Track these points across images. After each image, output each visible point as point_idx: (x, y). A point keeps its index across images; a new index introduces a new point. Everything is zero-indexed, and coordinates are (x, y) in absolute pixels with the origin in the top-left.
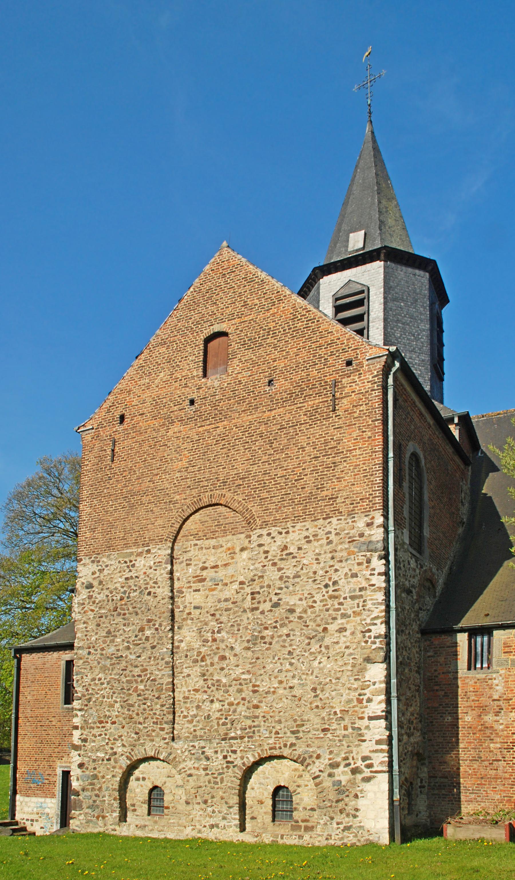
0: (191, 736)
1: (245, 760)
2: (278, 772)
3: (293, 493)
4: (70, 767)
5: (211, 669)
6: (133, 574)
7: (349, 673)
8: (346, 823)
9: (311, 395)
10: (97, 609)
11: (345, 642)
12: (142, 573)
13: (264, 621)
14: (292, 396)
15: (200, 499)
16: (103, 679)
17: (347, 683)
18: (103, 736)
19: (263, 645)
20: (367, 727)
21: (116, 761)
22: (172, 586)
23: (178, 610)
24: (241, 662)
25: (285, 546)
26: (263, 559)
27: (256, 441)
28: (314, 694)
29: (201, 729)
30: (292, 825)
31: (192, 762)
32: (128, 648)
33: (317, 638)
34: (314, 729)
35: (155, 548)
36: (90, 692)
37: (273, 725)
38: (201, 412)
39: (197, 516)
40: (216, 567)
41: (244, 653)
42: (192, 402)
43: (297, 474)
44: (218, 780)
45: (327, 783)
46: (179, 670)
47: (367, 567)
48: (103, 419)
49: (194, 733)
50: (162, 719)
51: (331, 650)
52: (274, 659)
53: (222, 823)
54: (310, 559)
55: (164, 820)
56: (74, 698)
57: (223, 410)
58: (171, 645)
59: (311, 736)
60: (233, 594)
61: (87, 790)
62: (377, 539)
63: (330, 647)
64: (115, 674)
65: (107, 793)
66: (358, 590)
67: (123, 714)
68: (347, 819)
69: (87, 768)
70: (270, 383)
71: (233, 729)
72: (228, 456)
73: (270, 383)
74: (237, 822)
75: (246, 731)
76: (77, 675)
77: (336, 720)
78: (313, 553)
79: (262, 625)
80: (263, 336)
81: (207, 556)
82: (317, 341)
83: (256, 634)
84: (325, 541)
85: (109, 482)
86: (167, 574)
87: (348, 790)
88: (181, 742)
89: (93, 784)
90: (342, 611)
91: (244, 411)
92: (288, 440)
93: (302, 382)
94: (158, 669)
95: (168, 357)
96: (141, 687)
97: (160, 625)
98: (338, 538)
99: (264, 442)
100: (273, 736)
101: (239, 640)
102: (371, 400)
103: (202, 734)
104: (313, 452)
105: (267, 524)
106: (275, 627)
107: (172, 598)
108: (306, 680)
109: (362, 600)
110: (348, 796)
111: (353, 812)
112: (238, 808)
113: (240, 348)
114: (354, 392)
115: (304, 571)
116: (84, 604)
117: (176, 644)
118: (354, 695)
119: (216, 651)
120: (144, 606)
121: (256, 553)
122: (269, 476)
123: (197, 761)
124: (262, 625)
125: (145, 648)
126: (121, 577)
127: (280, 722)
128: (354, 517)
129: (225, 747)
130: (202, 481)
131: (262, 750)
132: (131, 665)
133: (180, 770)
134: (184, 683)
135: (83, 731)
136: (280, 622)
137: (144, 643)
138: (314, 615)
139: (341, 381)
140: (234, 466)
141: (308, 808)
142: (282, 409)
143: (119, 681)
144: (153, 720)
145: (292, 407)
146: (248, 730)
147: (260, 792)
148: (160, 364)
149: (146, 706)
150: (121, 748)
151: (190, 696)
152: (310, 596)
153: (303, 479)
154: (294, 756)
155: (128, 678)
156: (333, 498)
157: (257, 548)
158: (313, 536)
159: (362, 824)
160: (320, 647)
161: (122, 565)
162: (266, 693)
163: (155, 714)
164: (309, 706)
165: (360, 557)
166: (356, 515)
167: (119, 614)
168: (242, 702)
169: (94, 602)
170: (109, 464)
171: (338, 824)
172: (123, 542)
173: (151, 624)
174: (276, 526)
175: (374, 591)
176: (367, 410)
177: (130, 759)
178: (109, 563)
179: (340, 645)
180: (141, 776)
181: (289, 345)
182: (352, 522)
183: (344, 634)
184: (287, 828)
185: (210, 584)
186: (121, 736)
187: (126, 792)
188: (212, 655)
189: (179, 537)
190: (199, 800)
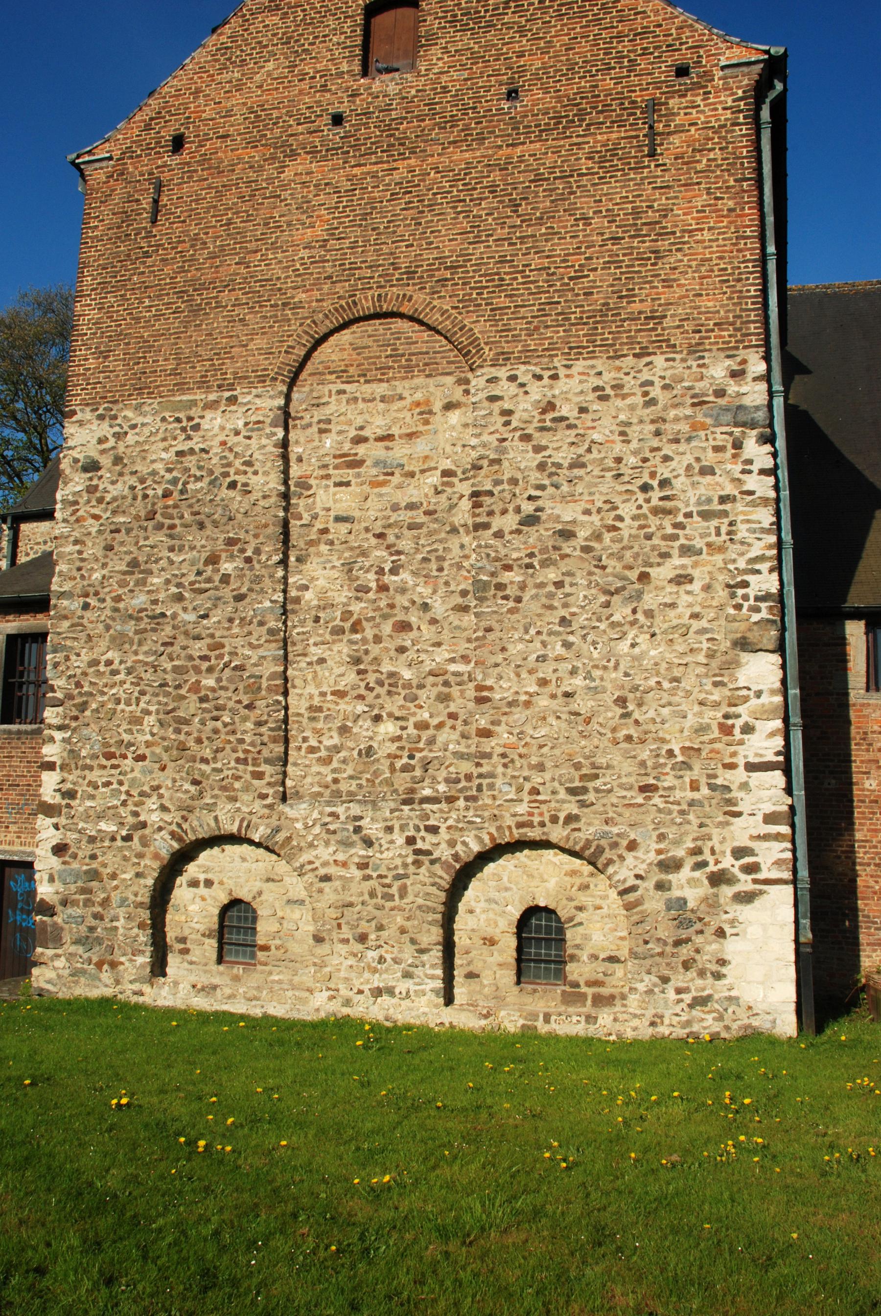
0: (327, 793)
1: (459, 848)
2: (531, 876)
3: (566, 301)
4: (32, 854)
5: (375, 650)
6: (196, 444)
7: (701, 670)
8: (696, 990)
9: (602, 123)
10: (108, 514)
11: (690, 605)
12: (216, 442)
13: (503, 552)
14: (560, 123)
15: (355, 303)
16: (117, 662)
17: (697, 689)
18: (115, 786)
19: (500, 602)
20: (744, 786)
21: (144, 842)
22: (286, 472)
23: (299, 523)
24: (446, 635)
25: (549, 402)
26: (499, 426)
27: (481, 199)
28: (620, 711)
29: (351, 777)
30: (564, 992)
31: (332, 849)
32: (179, 598)
33: (626, 593)
34: (621, 786)
35: (249, 393)
36: (86, 689)
37: (526, 773)
38: (359, 140)
39: (346, 336)
40: (389, 437)
41: (455, 619)
42: (338, 120)
43: (573, 266)
44: (394, 890)
45: (654, 903)
46: (299, 648)
47: (734, 456)
48: (134, 142)
49: (334, 787)
50: (259, 752)
51: (658, 620)
52: (527, 631)
53: (402, 986)
54: (607, 432)
55: (256, 975)
56: (47, 702)
57: (407, 138)
58: (281, 594)
59: (615, 800)
60: (426, 495)
61: (75, 903)
62: (755, 404)
63: (656, 613)
64: (146, 653)
65: (122, 912)
66: (716, 500)
67: (164, 739)
68: (699, 982)
69: (75, 856)
70: (512, 94)
71: (427, 781)
72: (420, 224)
73: (512, 94)
74: (439, 984)
75: (460, 786)
76: (55, 651)
77: (673, 769)
78: (612, 420)
79: (497, 559)
80: (493, 10)
81: (367, 416)
82: (613, 27)
83: (485, 578)
84: (639, 400)
85: (145, 263)
86: (275, 446)
87: (701, 919)
88: (304, 806)
89: (89, 892)
90: (682, 541)
91: (455, 142)
92: (552, 202)
93: (582, 98)
94: (250, 644)
95: (284, 34)
96: (210, 682)
97: (257, 551)
98: (668, 394)
99: (499, 202)
100: (526, 798)
102: (733, 142)
103: (353, 788)
104: (609, 228)
105: (509, 359)
106: (529, 566)
107: (286, 496)
108: (602, 679)
109: (726, 521)
110: (701, 932)
111: (714, 967)
112: (440, 954)
113: (445, 28)
114: (696, 124)
115: (595, 455)
116: (76, 503)
117: (293, 593)
118: (713, 717)
119: (386, 611)
120: (220, 511)
121: (483, 412)
122: (510, 267)
123: (341, 848)
124: (497, 559)
125: (219, 599)
126: (165, 450)
127: (541, 767)
128: (703, 358)
129: (410, 818)
130: (360, 268)
131: (499, 828)
132: (186, 633)
133: (302, 866)
135: (66, 775)
136: (539, 557)
137: (216, 589)
138: (618, 546)
139: (667, 104)
140: (432, 243)
141: (602, 956)
142: (538, 145)
143: (154, 667)
144: (235, 755)
145: (562, 143)
146: (463, 784)
147: (488, 920)
148: (266, 46)
149: (219, 724)
150: (157, 813)
151: (326, 706)
152: (608, 506)
153: (587, 276)
154: (576, 843)
155: (176, 663)
156: (656, 318)
157: (486, 404)
158: (613, 387)
159: (733, 993)
160: (634, 611)
161: (170, 427)
162: (510, 704)
164: (609, 735)
165: (718, 436)
166: (706, 354)
167: (159, 527)
168: (450, 722)
169: (100, 500)
170: (145, 228)
171: (679, 991)
172: (172, 381)
173: (236, 548)
174: (529, 363)
175: (753, 504)
176: (723, 159)
177: (180, 840)
178: (140, 420)
179: (680, 610)
180: (202, 877)
181: (553, 30)
182: (699, 366)
183: (688, 587)
184: (553, 999)
185: (374, 472)
186: (158, 787)
187: (165, 911)
188: (378, 620)
189: (304, 375)
190: (346, 932)
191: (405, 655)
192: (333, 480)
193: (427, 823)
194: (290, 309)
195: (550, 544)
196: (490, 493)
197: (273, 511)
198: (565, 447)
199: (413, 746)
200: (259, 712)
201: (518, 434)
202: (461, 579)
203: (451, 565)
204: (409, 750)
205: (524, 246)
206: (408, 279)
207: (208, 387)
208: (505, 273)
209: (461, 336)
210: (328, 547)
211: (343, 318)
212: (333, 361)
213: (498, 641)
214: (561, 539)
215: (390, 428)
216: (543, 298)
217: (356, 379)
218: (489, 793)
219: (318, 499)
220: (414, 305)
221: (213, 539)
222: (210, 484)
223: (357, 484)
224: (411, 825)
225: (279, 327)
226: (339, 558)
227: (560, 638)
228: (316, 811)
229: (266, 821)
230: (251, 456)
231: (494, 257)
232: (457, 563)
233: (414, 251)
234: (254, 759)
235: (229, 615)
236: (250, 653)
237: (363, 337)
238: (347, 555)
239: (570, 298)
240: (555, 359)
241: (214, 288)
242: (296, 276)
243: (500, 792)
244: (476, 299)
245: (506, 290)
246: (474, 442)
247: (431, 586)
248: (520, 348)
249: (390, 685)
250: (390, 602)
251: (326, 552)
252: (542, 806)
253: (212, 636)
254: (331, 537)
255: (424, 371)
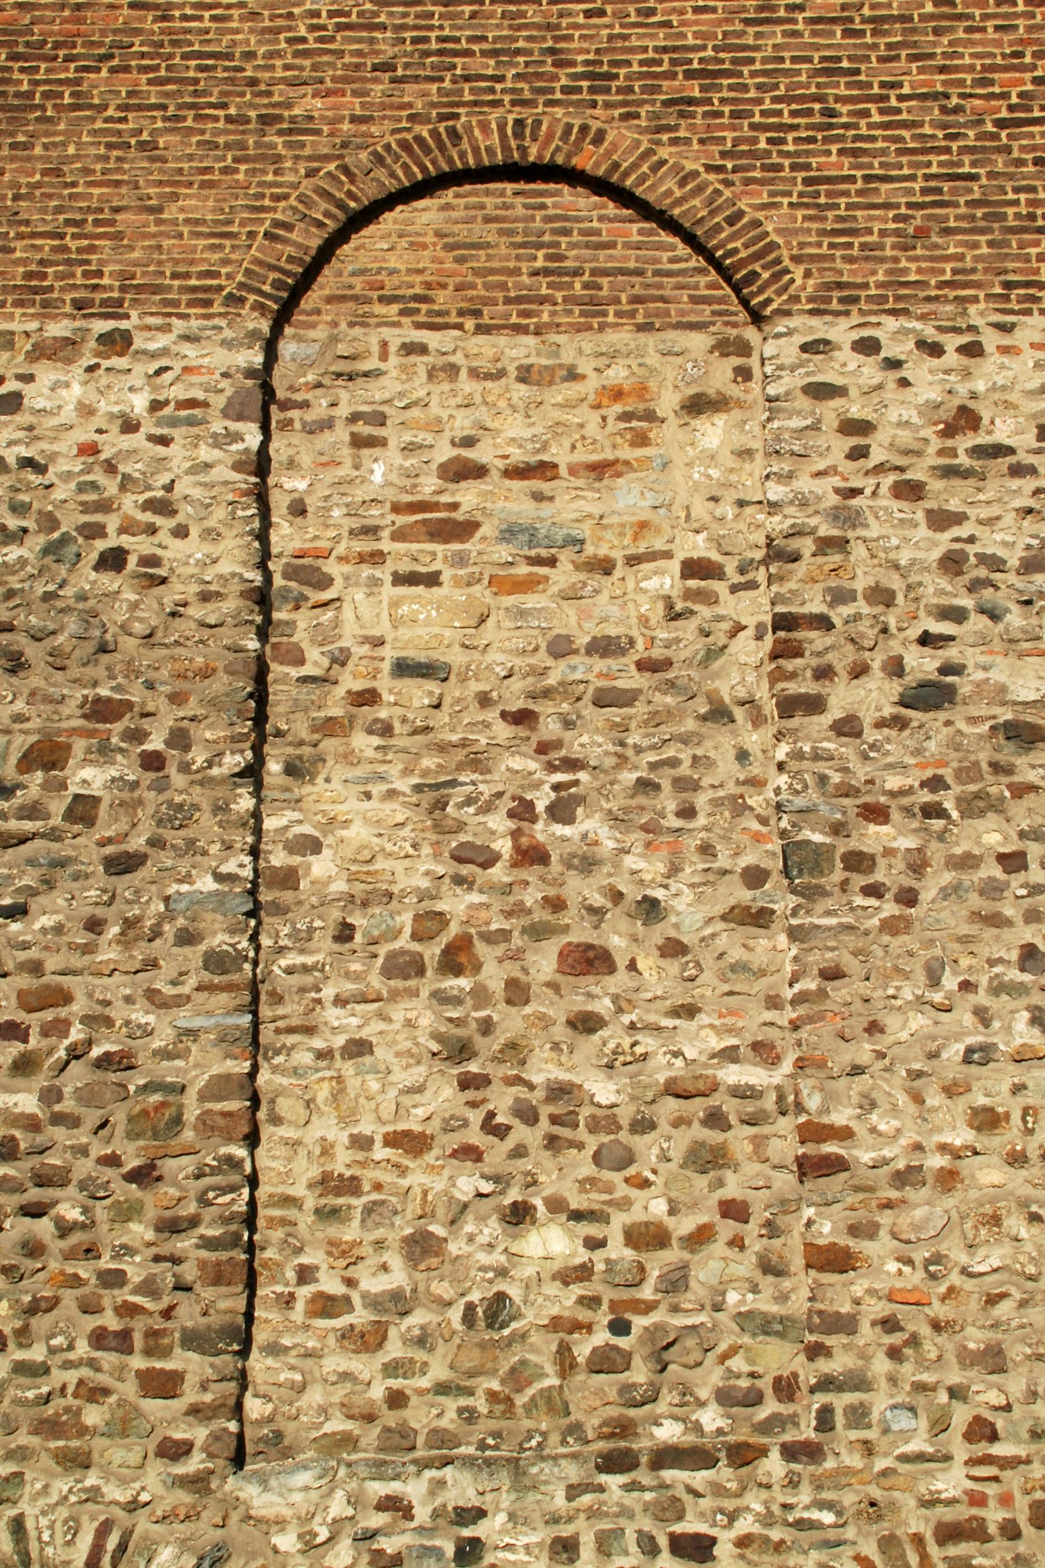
0: (371, 1436)
3: (991, 175)
12: (67, 445)
13: (861, 772)
15: (453, 133)
19: (859, 900)
22: (263, 536)
23: (294, 672)
29: (443, 1389)
35: (166, 329)
37: (955, 1377)
43: (1005, 96)
46: (292, 1010)
49: (391, 1418)
50: (167, 1313)
52: (934, 981)
58: (247, 859)
60: (644, 621)
71: (668, 1398)
75: (763, 1413)
79: (847, 791)
81: (482, 414)
83: (817, 838)
86: (238, 467)
88: (304, 1478)
94: (152, 995)
97: (180, 739)
100: (961, 1451)
101: (693, 868)
103: (449, 1421)
105: (856, 300)
117: (278, 858)
120: (72, 625)
121: (796, 423)
122: (849, 85)
124: (847, 791)
125: (61, 863)
129: (627, 1513)
130: (467, 53)
134: (323, 1093)
136: (957, 789)
137: (53, 835)
140: (652, 12)
144: (91, 1322)
146: (771, 1407)
149: (44, 1227)
151: (369, 1176)
157: (803, 402)
162: (905, 1178)
163: (114, 1279)
168: (727, 1228)
173: (118, 727)
174: (906, 312)
189: (311, 299)
191: (596, 1038)
192: (390, 567)
193: (678, 1528)
194: (280, 133)
195: (983, 757)
196: (824, 623)
197: (228, 636)
198: (1009, 519)
199: (625, 1294)
200: (173, 1192)
201: (888, 480)
202: (745, 839)
203: (716, 802)
204: (614, 1305)
205: (883, 41)
206: (592, 90)
207: (45, 304)
208: (838, 99)
209: (733, 237)
210: (376, 741)
211: (423, 169)
212: (392, 272)
213: (858, 1006)
214: (1010, 747)
215: (545, 447)
216: (936, 164)
217: (454, 319)
218: (854, 1435)
219: (347, 613)
220: (608, 153)
221: (49, 700)
222: (46, 551)
223: (457, 582)
224: (631, 1536)
225: (253, 172)
226: (407, 772)
227: (1024, 1001)
228: (339, 1494)
229: (181, 1529)
230: (169, 488)
231: (809, 60)
232: (733, 798)
233: (605, 28)
234: (152, 1334)
235: (89, 911)
236: (151, 1018)
237: (472, 220)
238: (428, 762)
239: (1000, 167)
240: (972, 309)
241: (68, 59)
242: (297, 54)
243: (886, 1431)
244: (768, 153)
245: (840, 138)
246: (776, 492)
247: (664, 853)
248: (881, 277)
249: (554, 1120)
250: (552, 892)
251: (370, 753)
252: (1007, 1474)
253: (36, 968)
254: (383, 714)
255: (633, 314)
